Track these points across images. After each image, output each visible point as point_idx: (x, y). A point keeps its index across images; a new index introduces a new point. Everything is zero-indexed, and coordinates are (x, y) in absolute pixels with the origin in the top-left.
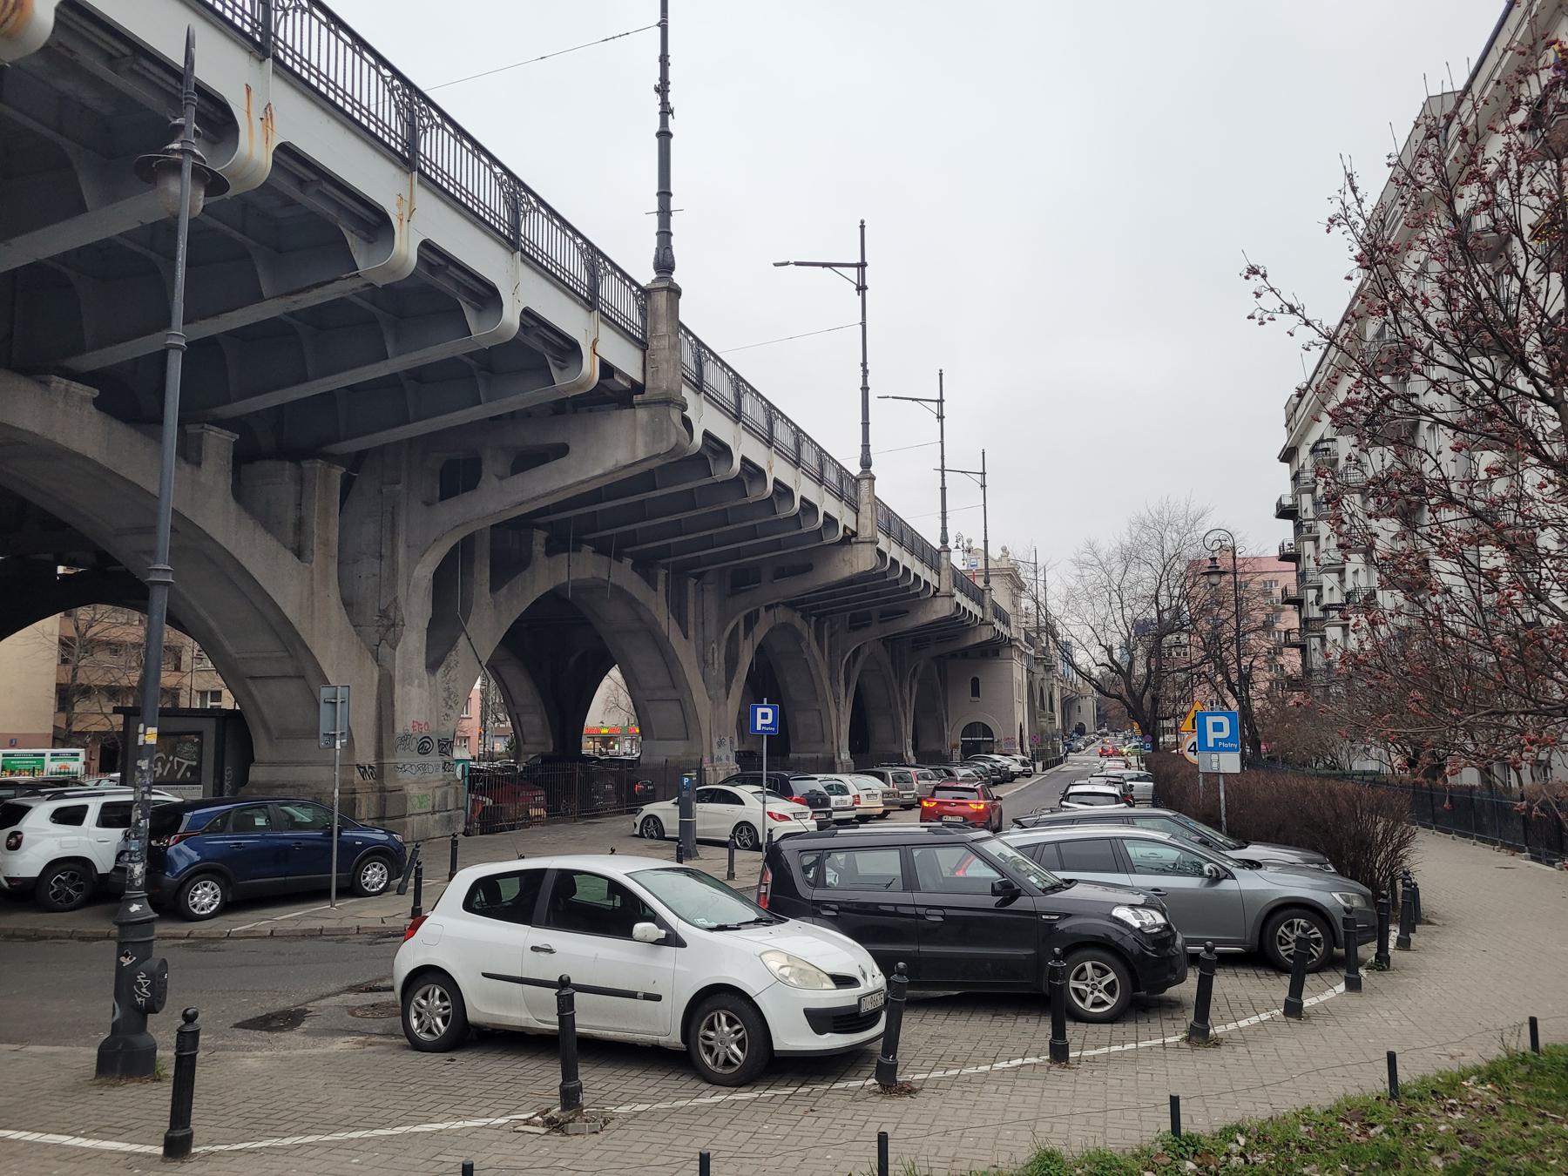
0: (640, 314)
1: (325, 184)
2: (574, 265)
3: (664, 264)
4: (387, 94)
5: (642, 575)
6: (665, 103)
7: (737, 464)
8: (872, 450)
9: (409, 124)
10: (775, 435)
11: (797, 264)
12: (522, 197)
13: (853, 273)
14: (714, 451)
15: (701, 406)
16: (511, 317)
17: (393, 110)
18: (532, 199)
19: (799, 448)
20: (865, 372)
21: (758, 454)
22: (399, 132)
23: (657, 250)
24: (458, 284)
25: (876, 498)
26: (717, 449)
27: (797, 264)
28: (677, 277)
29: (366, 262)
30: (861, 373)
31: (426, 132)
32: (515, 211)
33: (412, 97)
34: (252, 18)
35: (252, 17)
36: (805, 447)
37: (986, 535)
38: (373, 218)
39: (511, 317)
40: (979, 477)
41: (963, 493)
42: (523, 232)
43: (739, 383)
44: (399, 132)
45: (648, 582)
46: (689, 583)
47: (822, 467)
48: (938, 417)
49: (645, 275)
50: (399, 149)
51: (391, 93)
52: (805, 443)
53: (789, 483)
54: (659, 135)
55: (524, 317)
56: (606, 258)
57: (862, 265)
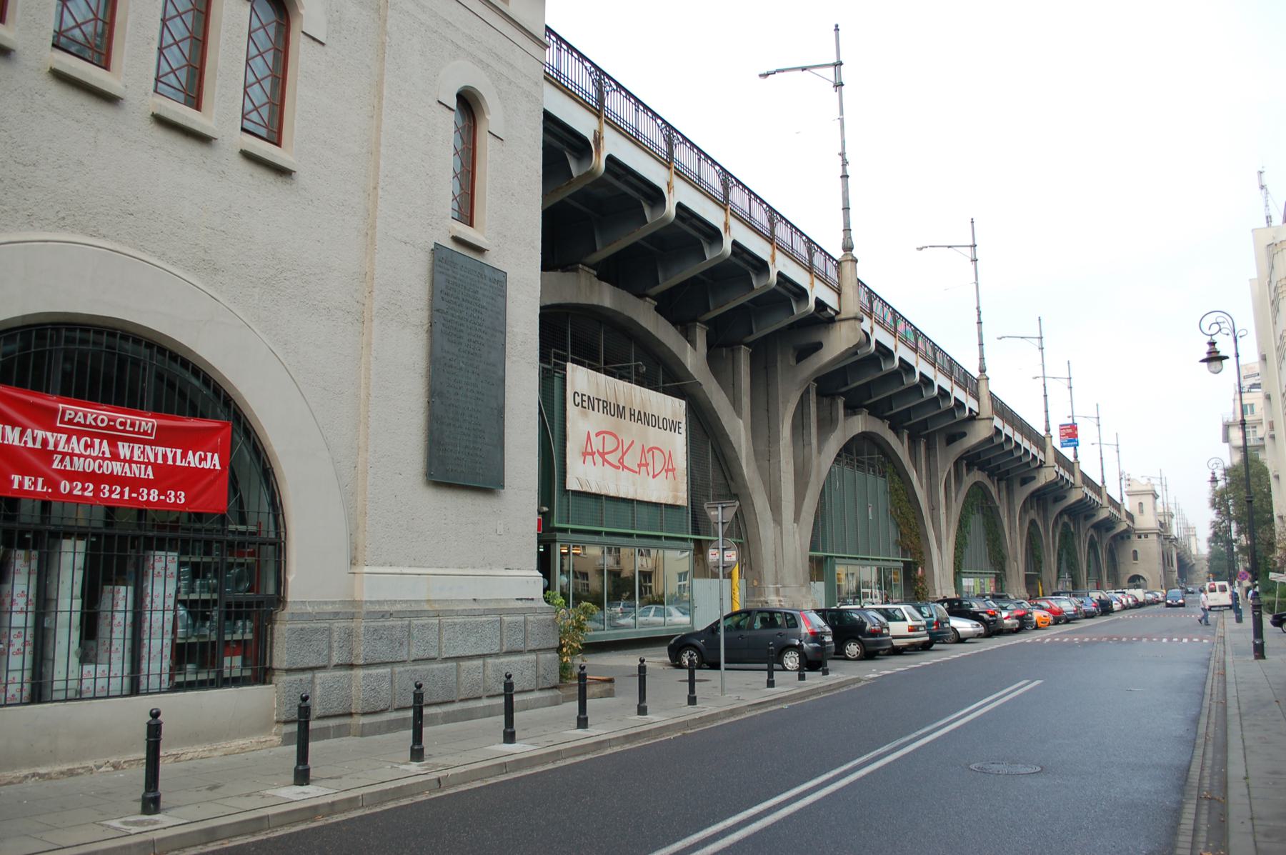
0: (808, 252)
1: (694, 220)
2: (586, 83)
3: (848, 248)
4: (588, 75)
5: (681, 332)
6: (768, 74)
7: (773, 277)
8: (986, 361)
9: (599, 91)
10: (776, 233)
11: (930, 246)
12: (674, 136)
13: (968, 251)
14: (905, 370)
15: (813, 281)
16: (671, 209)
17: (663, 139)
18: (679, 137)
19: (935, 354)
20: (845, 163)
21: (929, 372)
22: (594, 96)
23: (844, 239)
24: (789, 291)
25: (859, 280)
26: (884, 352)
27: (930, 246)
28: (855, 253)
29: (710, 254)
30: (977, 313)
31: (608, 94)
32: (670, 143)
33: (600, 76)
34: (572, 81)
35: (595, 99)
36: (876, 303)
37: (1045, 390)
38: (758, 264)
39: (671, 209)
40: (1066, 381)
41: (1058, 392)
42: (606, 105)
43: (935, 347)
44: (594, 96)
45: (898, 437)
46: (839, 401)
47: (951, 368)
48: (972, 261)
49: (838, 253)
50: (594, 104)
51: (590, 75)
52: (920, 338)
53: (963, 400)
54: (978, 323)
55: (779, 278)
56: (777, 213)
57: (839, 64)
